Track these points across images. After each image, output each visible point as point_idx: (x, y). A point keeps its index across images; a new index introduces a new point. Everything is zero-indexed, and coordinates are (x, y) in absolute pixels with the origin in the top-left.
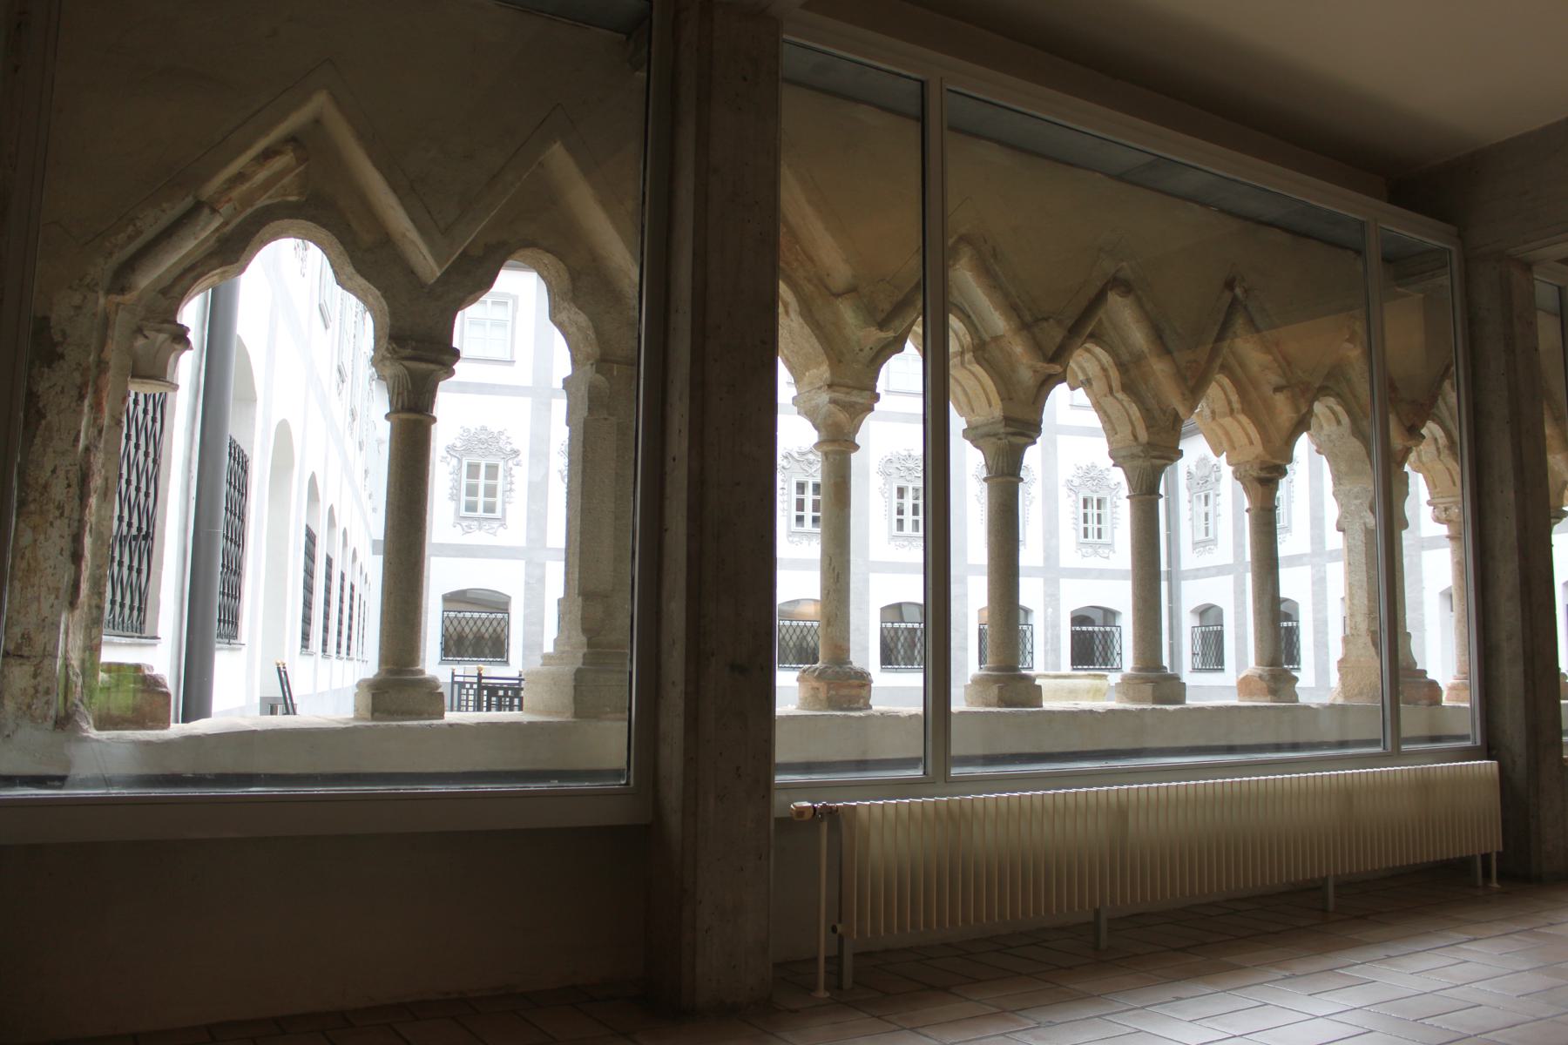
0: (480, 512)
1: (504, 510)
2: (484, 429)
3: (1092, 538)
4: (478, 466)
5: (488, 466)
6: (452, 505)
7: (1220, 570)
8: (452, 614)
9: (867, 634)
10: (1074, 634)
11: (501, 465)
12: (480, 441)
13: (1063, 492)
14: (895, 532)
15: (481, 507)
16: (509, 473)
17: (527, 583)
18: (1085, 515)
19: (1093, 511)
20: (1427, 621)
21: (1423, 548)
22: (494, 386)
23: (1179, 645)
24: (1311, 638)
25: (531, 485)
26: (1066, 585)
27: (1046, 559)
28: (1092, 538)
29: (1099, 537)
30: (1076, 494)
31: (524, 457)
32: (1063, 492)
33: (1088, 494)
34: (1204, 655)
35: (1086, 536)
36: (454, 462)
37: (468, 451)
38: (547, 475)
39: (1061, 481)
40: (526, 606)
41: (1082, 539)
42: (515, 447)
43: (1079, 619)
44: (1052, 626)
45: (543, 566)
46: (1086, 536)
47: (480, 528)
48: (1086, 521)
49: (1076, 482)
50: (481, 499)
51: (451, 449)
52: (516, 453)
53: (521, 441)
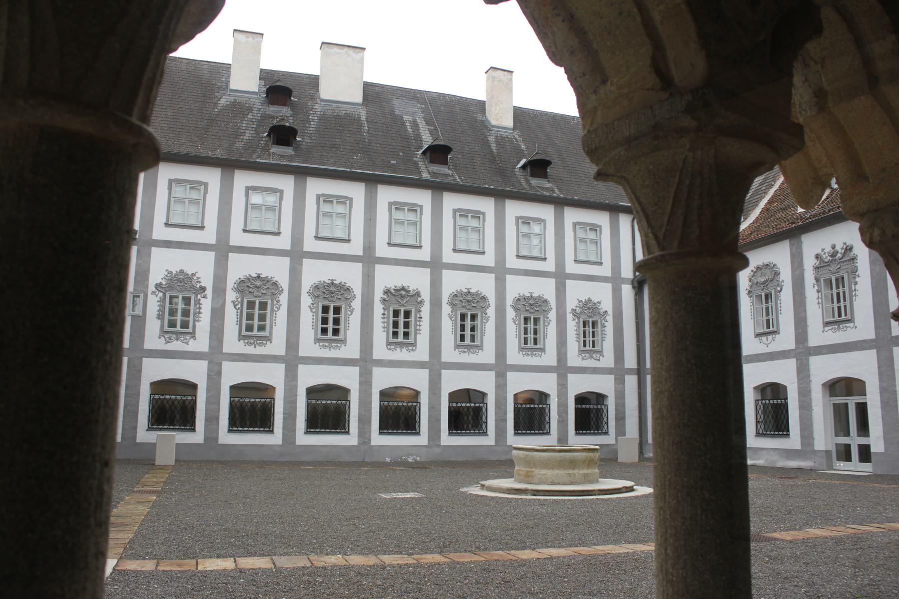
0: (178, 328)
1: (194, 326)
2: (182, 271)
3: (530, 344)
4: (254, 302)
5: (260, 303)
6: (159, 322)
7: (274, 359)
8: (157, 397)
9: (440, 411)
10: (576, 410)
11: (193, 297)
12: (179, 280)
13: (569, 317)
14: (459, 342)
15: (256, 328)
16: (198, 302)
17: (209, 375)
18: (584, 332)
19: (531, 326)
20: (814, 403)
21: (810, 354)
22: (190, 244)
23: (646, 417)
24: (494, 418)
25: (213, 311)
26: (377, 372)
27: (559, 361)
28: (530, 344)
29: (594, 346)
30: (578, 318)
31: (209, 292)
32: (569, 317)
33: (587, 319)
34: (766, 422)
35: (585, 346)
36: (161, 294)
37: (170, 287)
38: (224, 304)
39: (569, 310)
40: (208, 391)
41: (582, 348)
42: (203, 285)
43: (581, 399)
44: (563, 407)
45: (220, 365)
46: (585, 346)
47: (177, 340)
48: (584, 336)
49: (578, 310)
50: (330, 326)
51: (158, 286)
52: (203, 289)
53: (207, 281)
